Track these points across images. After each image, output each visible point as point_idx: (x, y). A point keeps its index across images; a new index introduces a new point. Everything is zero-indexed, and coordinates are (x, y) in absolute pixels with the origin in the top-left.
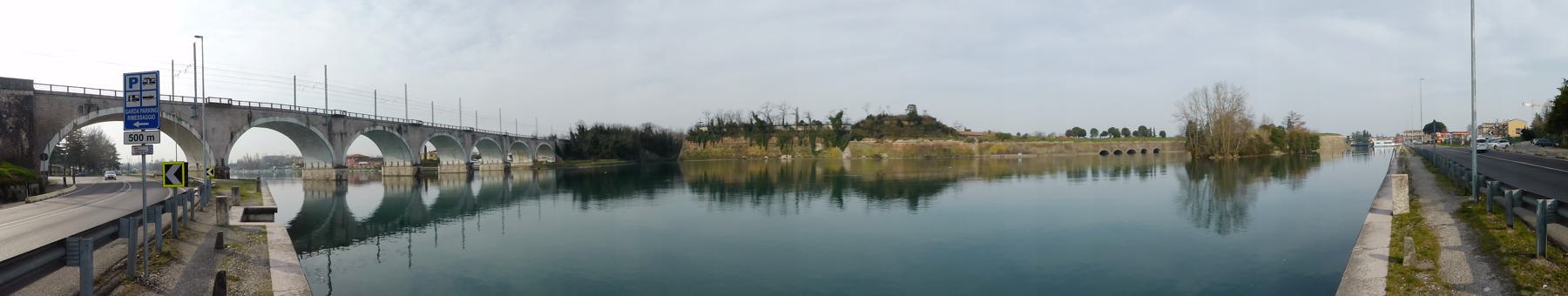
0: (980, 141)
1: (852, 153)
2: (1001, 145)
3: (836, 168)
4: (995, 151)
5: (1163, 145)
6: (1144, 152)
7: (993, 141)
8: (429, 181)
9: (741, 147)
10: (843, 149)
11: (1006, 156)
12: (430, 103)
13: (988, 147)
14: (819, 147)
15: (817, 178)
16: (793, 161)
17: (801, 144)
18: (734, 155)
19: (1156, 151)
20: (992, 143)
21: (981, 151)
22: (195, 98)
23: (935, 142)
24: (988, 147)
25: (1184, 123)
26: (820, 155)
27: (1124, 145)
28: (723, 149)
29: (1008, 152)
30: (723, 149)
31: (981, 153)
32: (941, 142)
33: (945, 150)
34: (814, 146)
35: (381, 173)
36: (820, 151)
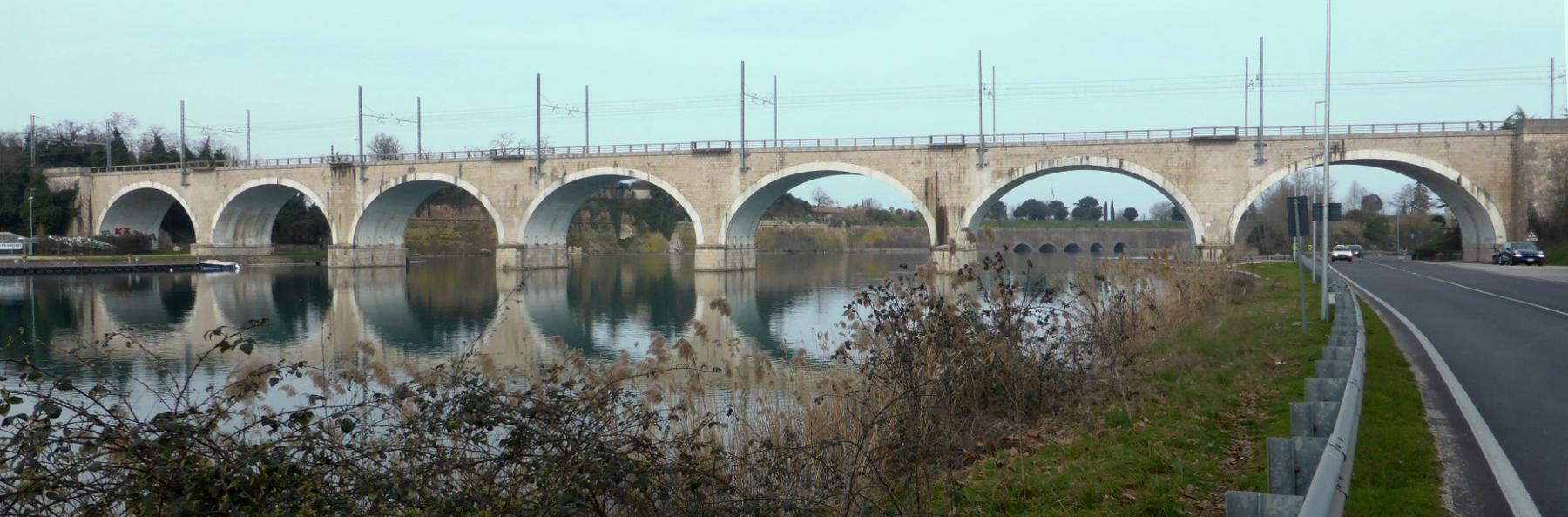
0: (848, 225)
1: (683, 244)
2: (878, 231)
3: (655, 269)
4: (872, 243)
5: (1133, 237)
6: (1095, 249)
7: (866, 224)
8: (82, 446)
9: (475, 227)
10: (668, 236)
11: (889, 250)
12: (1050, 191)
13: (860, 234)
14: (627, 232)
15: (623, 289)
16: (585, 259)
17: (594, 227)
18: (462, 245)
19: (1119, 248)
20: (868, 227)
21: (852, 240)
22: (982, 137)
23: (795, 225)
24: (860, 234)
25: (204, 138)
26: (632, 247)
27: (1058, 235)
28: (432, 230)
29: (891, 245)
30: (432, 230)
31: (851, 246)
32: (802, 224)
33: (809, 240)
34: (618, 229)
35: (41, 493)
36: (630, 240)
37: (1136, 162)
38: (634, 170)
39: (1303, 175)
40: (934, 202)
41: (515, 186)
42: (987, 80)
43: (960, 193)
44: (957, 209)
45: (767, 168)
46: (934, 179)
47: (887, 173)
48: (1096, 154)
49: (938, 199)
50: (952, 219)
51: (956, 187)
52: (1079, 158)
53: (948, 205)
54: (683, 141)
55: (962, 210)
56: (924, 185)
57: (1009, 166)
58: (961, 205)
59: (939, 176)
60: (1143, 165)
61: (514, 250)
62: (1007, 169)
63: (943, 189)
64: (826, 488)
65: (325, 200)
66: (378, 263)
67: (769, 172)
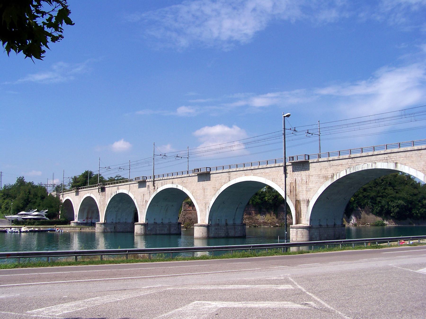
37: (405, 164)
38: (178, 185)
39: (112, 222)
40: (294, 197)
41: (144, 195)
42: (410, 121)
43: (307, 191)
44: (306, 201)
45: (224, 181)
46: (294, 183)
47: (272, 181)
48: (380, 161)
49: (296, 195)
50: (303, 207)
51: (305, 188)
52: (370, 164)
53: (301, 199)
54: (218, 166)
55: (308, 202)
56: (289, 187)
57: (332, 172)
58: (308, 199)
59: (297, 181)
60: (410, 167)
61: (141, 225)
62: (331, 174)
63: (299, 189)
64: (367, 297)
65: (99, 202)
66: (118, 230)
67: (225, 183)
